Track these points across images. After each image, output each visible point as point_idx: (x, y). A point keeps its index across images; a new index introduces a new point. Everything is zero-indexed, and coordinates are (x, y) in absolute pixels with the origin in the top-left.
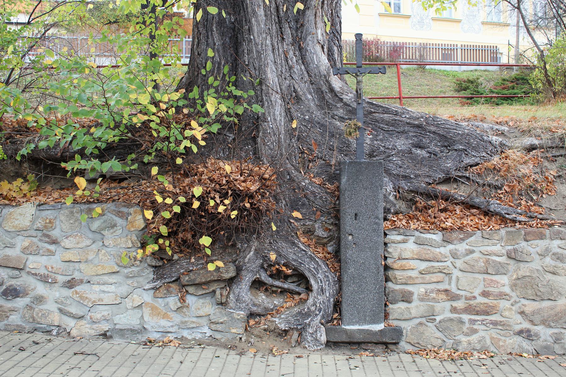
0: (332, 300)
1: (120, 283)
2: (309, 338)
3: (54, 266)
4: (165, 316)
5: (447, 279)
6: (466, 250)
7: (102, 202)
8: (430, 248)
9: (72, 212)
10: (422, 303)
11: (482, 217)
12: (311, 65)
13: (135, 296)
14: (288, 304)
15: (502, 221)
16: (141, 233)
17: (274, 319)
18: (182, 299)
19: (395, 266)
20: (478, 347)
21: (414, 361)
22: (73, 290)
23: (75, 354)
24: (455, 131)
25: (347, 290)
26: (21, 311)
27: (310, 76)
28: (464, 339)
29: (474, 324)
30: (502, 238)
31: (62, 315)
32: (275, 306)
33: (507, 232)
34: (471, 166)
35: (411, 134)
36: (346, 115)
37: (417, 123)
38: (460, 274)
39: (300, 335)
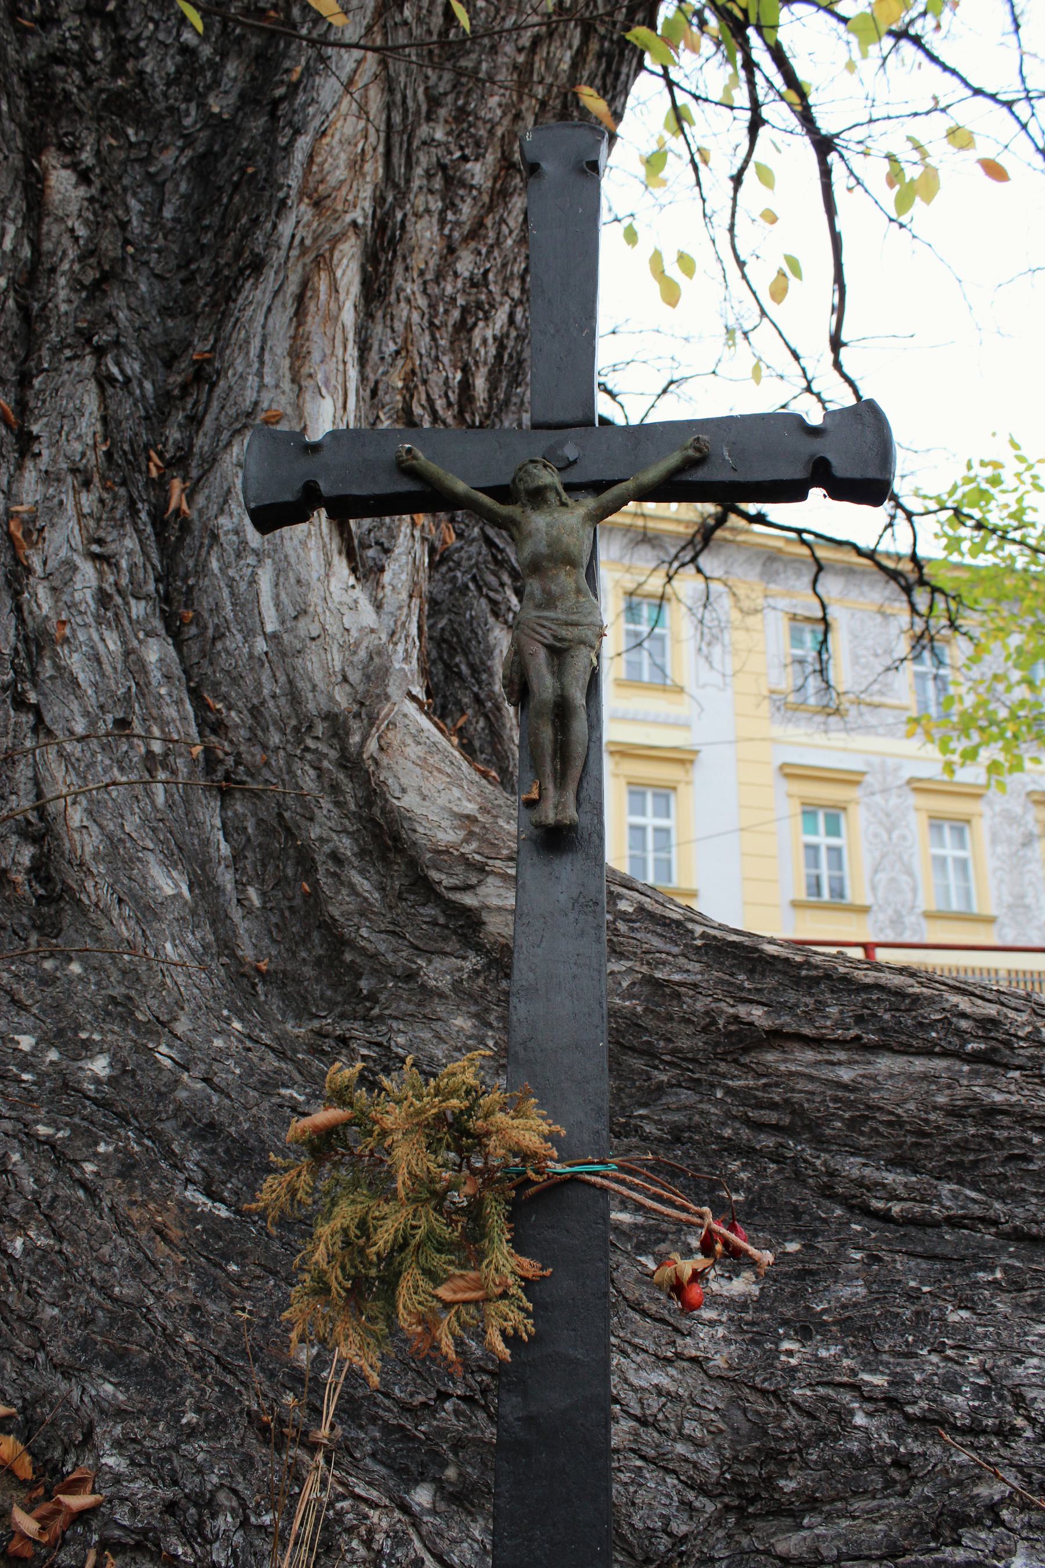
12: (235, 641)
27: (211, 724)
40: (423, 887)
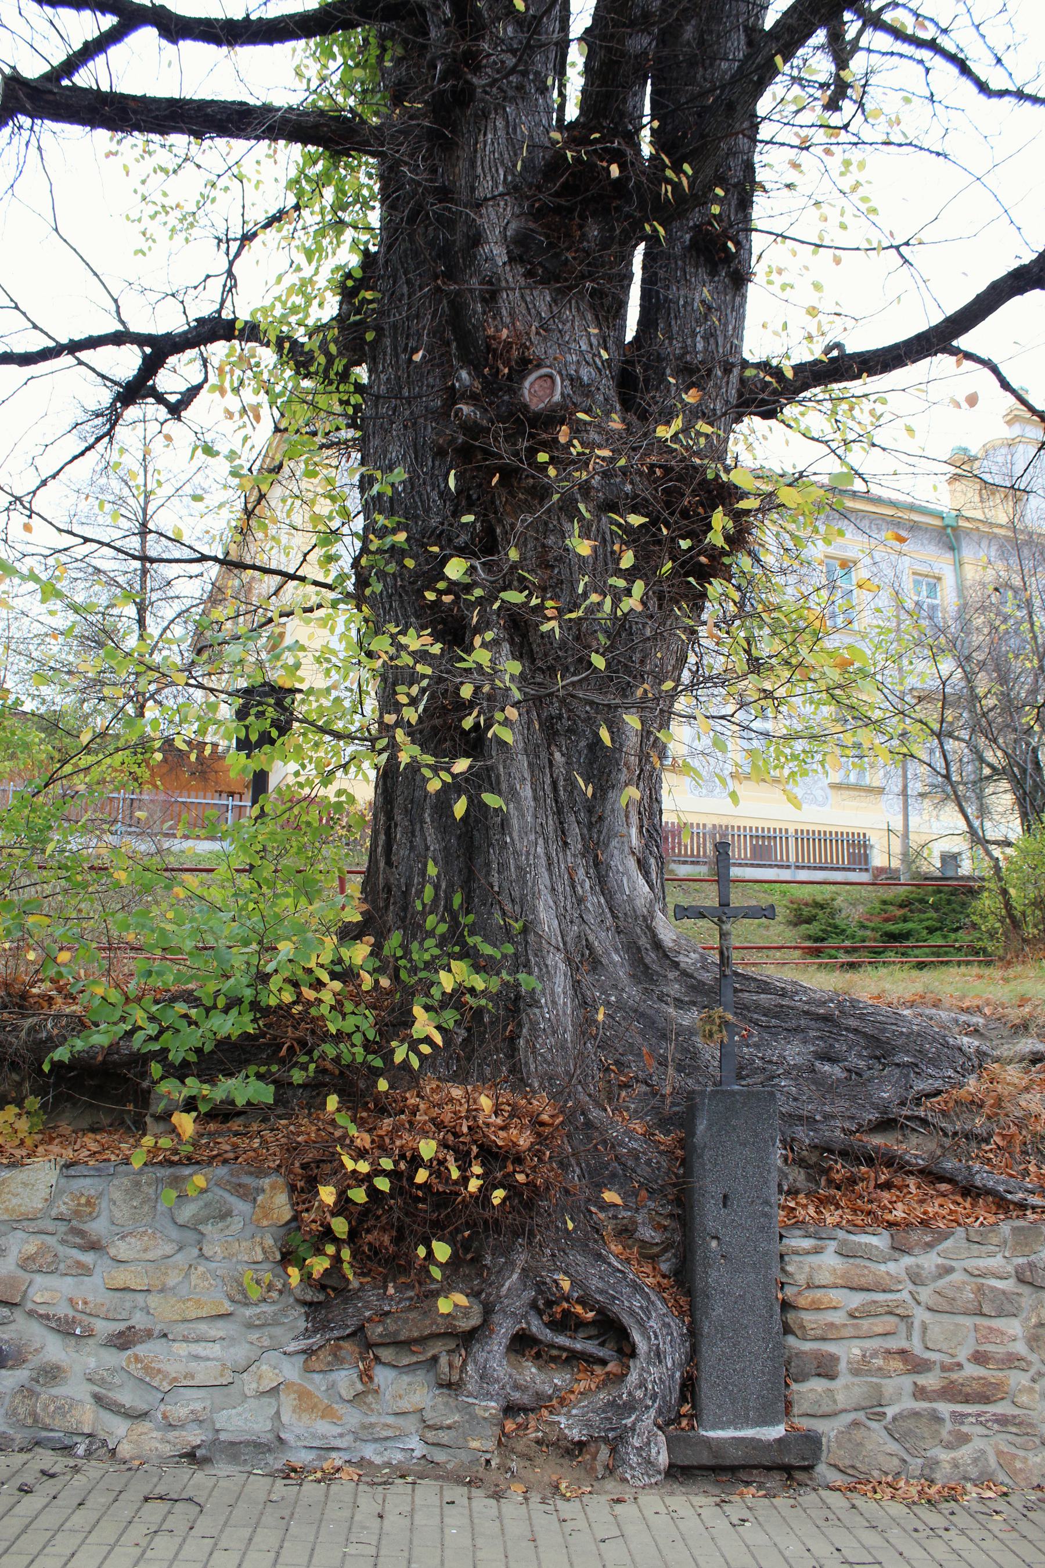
0: (678, 1374)
1: (233, 1339)
2: (634, 1459)
3: (90, 1299)
4: (327, 1413)
6: (937, 1266)
7: (198, 1163)
8: (868, 1263)
9: (137, 1184)
11: (960, 1200)
13: (264, 1367)
14: (582, 1385)
15: (999, 1207)
16: (283, 1231)
17: (557, 1418)
18: (366, 1376)
19: (802, 1302)
20: (974, 1472)
21: (854, 1507)
22: (129, 1352)
23: (146, 1499)
25: (711, 1353)
26: (7, 1400)
27: (615, 917)
28: (945, 1456)
30: (1005, 1242)
31: (101, 1411)
32: (556, 1388)
33: (1014, 1229)
34: (928, 1096)
35: (812, 1033)
36: (687, 994)
38: (927, 1316)
39: (614, 1451)
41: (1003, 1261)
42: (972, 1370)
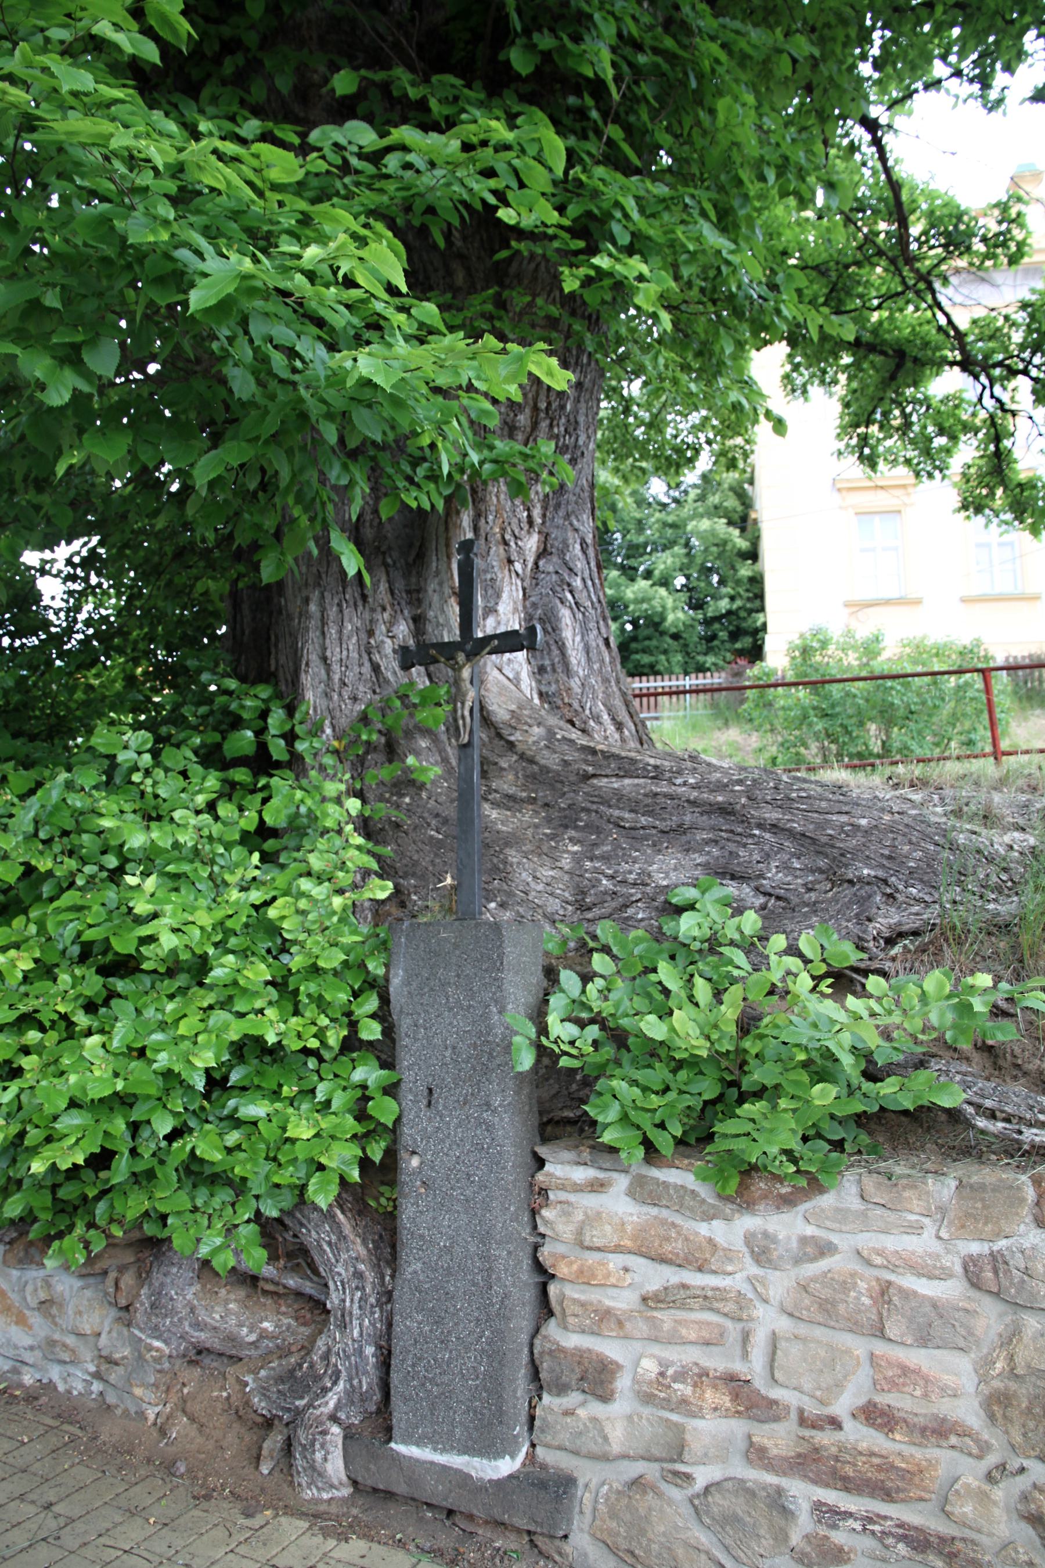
5: (733, 1330)
6: (804, 1240)
10: (647, 1411)
24: (844, 818)
29: (834, 1527)
37: (720, 799)
40: (499, 736)
41: (936, 1247)
42: (858, 1435)
